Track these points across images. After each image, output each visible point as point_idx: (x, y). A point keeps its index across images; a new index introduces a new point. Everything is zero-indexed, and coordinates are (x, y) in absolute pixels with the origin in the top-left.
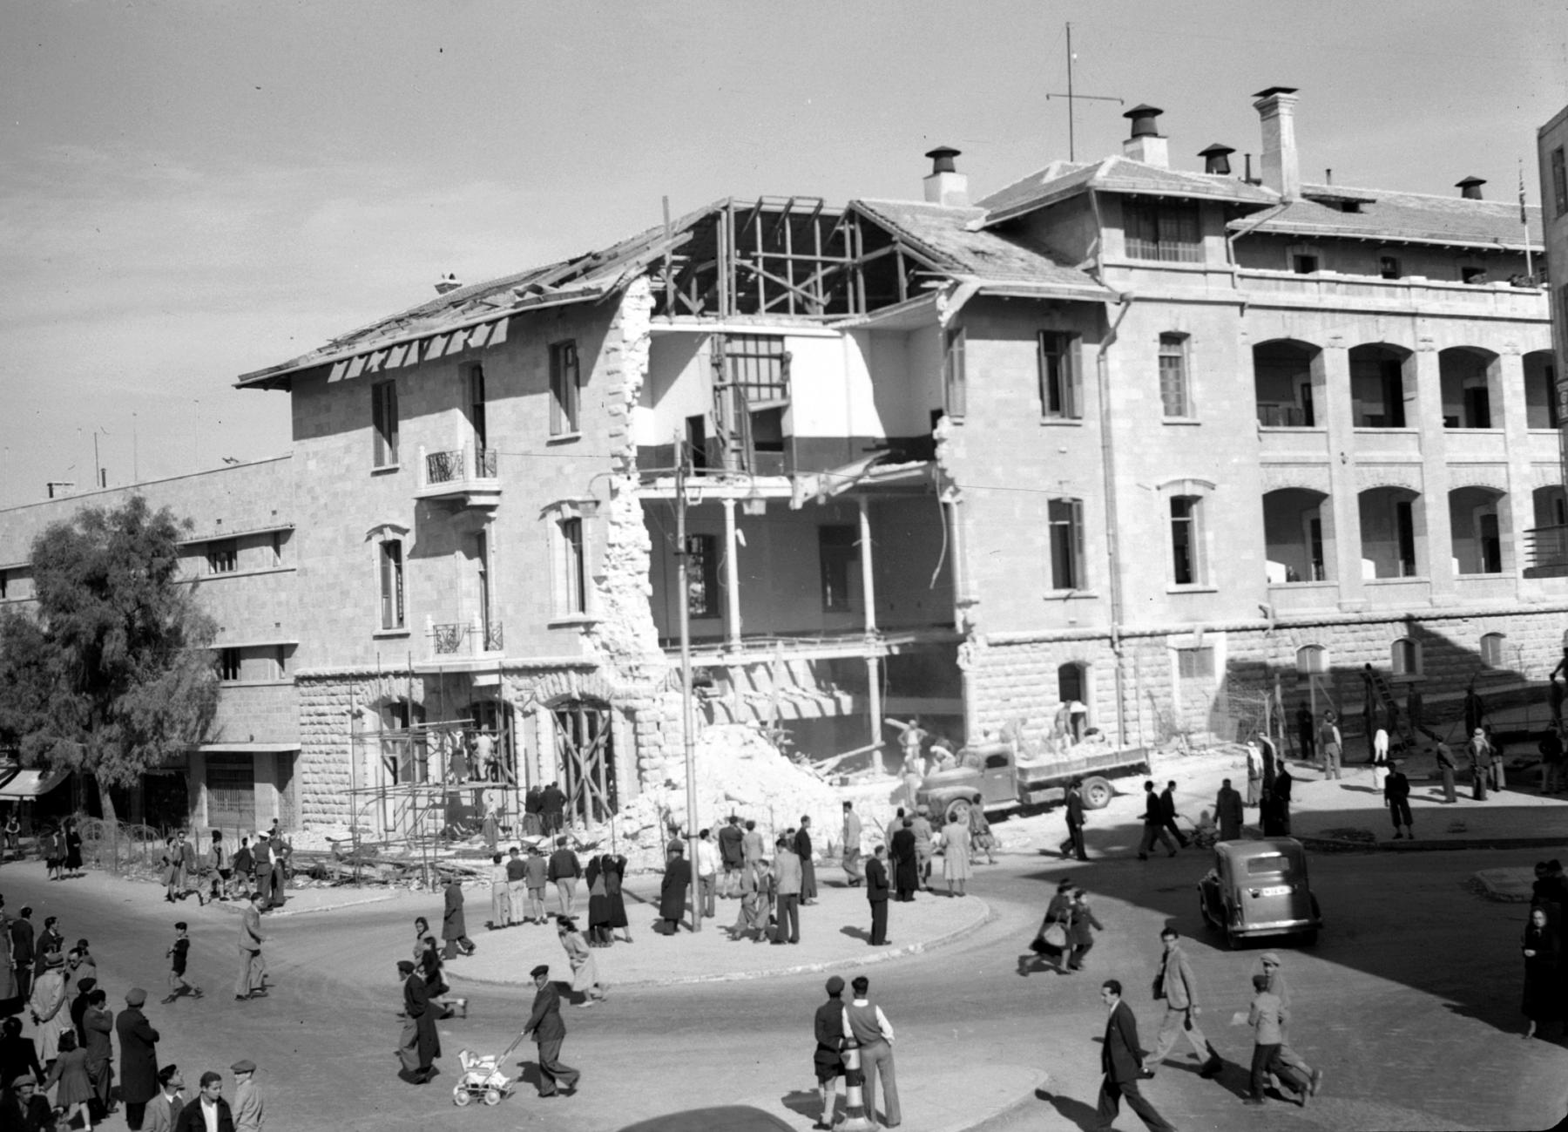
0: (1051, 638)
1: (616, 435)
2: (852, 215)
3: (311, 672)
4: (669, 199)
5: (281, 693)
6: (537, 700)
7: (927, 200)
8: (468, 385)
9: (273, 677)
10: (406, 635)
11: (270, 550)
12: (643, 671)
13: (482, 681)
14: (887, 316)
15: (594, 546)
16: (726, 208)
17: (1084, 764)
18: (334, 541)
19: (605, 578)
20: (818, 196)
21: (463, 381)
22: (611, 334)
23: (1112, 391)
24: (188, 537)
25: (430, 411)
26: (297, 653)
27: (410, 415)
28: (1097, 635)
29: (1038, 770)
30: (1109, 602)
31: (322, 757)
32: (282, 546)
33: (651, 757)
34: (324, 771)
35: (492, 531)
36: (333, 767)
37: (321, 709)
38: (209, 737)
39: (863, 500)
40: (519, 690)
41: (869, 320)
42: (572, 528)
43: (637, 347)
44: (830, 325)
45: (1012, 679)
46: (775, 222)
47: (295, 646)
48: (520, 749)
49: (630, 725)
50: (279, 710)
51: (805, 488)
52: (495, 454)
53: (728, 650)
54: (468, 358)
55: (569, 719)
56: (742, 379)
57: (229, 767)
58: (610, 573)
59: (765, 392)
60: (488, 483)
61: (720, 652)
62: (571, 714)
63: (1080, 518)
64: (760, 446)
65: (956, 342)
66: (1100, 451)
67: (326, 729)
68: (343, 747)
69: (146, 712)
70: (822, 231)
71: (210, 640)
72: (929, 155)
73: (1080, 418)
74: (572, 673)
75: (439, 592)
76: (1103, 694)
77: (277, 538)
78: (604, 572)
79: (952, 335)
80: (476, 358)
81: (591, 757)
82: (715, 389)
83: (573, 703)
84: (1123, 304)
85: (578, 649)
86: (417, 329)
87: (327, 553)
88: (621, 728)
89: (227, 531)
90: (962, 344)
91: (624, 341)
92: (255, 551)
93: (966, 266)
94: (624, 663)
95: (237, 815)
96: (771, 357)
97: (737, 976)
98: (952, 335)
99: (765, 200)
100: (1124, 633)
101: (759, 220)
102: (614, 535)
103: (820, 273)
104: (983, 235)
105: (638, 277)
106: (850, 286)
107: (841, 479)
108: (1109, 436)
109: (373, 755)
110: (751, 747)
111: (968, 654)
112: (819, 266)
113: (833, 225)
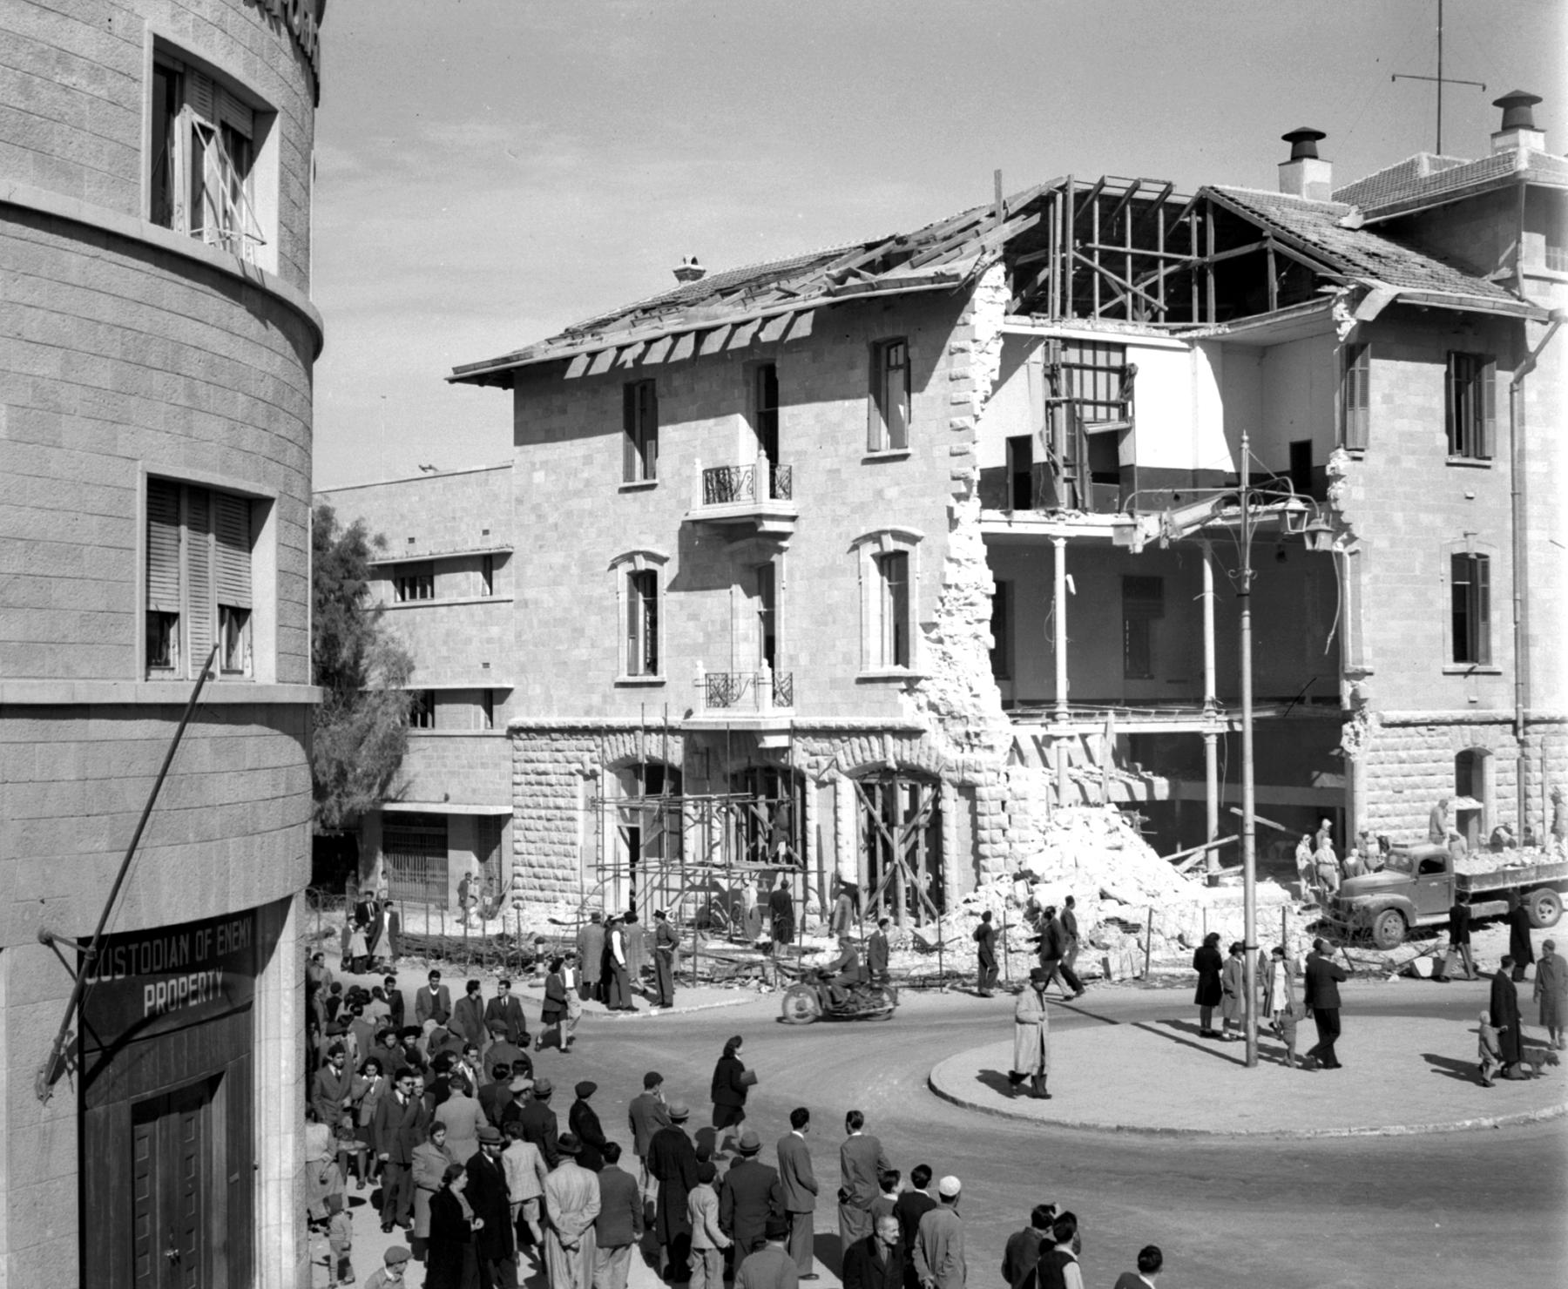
0: (1450, 719)
1: (961, 454)
2: (1202, 204)
3: (531, 722)
4: (1003, 173)
5: (488, 745)
6: (838, 768)
7: (1281, 191)
8: (752, 389)
9: (477, 726)
10: (661, 684)
11: (477, 577)
12: (985, 740)
13: (771, 742)
14: (1251, 328)
15: (922, 587)
16: (1063, 189)
17: (1533, 873)
18: (565, 568)
19: (935, 625)
20: (1167, 180)
21: (747, 383)
22: (958, 332)
23: (1528, 428)
24: (379, 556)
25: (703, 415)
26: (512, 698)
27: (673, 420)
28: (1500, 719)
29: (1483, 878)
30: (1513, 680)
31: (540, 824)
32: (495, 573)
33: (993, 842)
34: (543, 840)
35: (784, 565)
36: (555, 836)
37: (541, 767)
38: (391, 791)
39: (1207, 546)
40: (812, 754)
41: (1228, 330)
42: (894, 566)
43: (989, 349)
44: (1178, 335)
45: (1406, 767)
46: (1112, 209)
47: (508, 691)
48: (812, 825)
49: (964, 804)
50: (483, 765)
51: (1147, 529)
52: (790, 471)
53: (1052, 717)
54: (757, 355)
55: (878, 792)
56: (1076, 395)
57: (414, 830)
58: (944, 621)
59: (1102, 411)
60: (782, 506)
61: (1044, 720)
62: (882, 787)
63: (1486, 578)
64: (1097, 477)
65: (1358, 361)
66: (1510, 498)
67: (547, 790)
68: (571, 813)
69: (330, 761)
70: (1165, 222)
71: (403, 680)
72: (1286, 138)
73: (1489, 458)
74: (888, 738)
75: (708, 635)
76: (1504, 789)
77: (489, 563)
78: (935, 618)
79: (1353, 352)
80: (768, 356)
81: (905, 841)
82: (1048, 404)
83: (884, 772)
84: (1551, 324)
85: (899, 709)
86: (695, 318)
87: (556, 582)
88: (954, 809)
89: (422, 552)
90: (1366, 363)
91: (975, 341)
92: (459, 577)
93: (1366, 269)
94: (958, 729)
95: (421, 887)
96: (1110, 370)
97: (1396, 1130)
98: (1353, 352)
99: (1108, 181)
100: (1532, 718)
101: (1096, 205)
102: (952, 574)
103: (1163, 271)
104: (1363, 234)
105: (993, 264)
106: (1195, 289)
107: (1188, 518)
108: (1522, 482)
109: (612, 825)
110: (1117, 834)
111: (1357, 734)
112: (1161, 263)
113: (1177, 216)
